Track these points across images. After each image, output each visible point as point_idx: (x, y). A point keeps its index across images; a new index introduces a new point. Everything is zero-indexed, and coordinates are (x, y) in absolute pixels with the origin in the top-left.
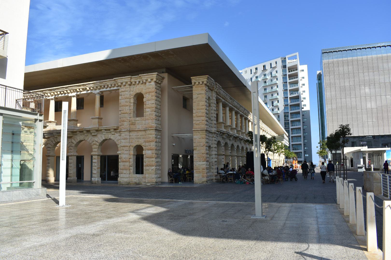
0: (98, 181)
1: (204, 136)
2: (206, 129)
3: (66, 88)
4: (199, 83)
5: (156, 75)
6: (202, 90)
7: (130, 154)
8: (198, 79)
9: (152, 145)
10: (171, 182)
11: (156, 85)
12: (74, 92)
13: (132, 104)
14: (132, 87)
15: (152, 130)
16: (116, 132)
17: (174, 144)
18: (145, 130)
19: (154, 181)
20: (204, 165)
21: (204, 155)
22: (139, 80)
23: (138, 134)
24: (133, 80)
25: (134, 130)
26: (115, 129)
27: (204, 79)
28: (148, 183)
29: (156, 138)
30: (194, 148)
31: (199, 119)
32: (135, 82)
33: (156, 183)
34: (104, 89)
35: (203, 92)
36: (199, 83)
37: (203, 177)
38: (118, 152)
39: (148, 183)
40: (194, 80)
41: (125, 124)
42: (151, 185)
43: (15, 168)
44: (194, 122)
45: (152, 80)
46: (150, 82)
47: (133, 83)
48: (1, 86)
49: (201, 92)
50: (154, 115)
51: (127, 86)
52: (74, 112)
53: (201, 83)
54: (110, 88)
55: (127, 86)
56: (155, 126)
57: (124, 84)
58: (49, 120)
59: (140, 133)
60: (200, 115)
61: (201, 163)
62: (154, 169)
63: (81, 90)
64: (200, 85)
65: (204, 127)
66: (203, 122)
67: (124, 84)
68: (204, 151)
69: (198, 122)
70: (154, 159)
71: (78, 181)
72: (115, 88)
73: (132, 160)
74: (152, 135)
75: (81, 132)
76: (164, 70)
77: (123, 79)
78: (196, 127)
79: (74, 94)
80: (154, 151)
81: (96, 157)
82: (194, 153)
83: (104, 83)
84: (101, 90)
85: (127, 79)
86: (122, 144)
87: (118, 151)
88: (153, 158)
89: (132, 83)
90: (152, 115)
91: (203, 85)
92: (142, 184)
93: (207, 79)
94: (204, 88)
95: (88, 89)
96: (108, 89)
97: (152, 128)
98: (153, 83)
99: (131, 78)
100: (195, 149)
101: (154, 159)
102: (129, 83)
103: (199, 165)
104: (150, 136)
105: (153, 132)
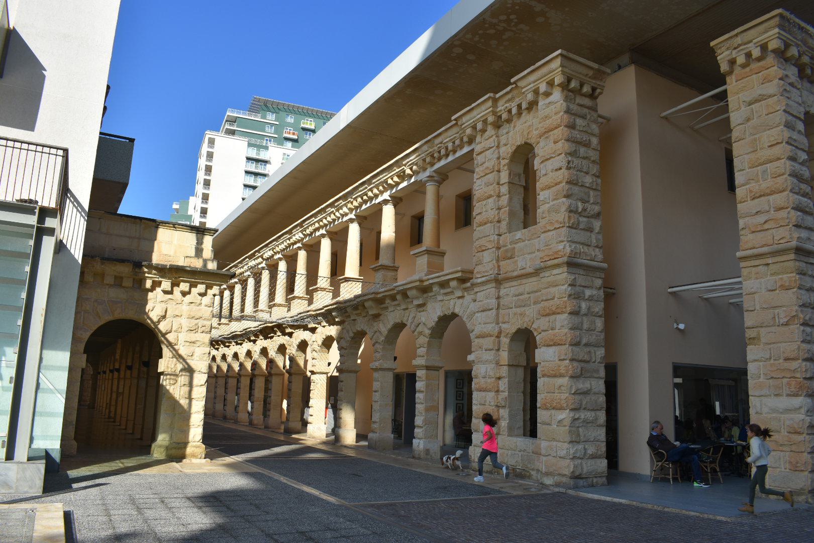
0: (427, 451)
1: (789, 277)
2: (794, 243)
3: (369, 182)
4: (749, 55)
5: (558, 62)
6: (767, 80)
7: (498, 364)
8: (739, 40)
9: (558, 325)
10: (660, 478)
11: (566, 99)
12: (385, 190)
13: (504, 189)
14: (503, 131)
15: (557, 266)
16: (466, 289)
17: (682, 326)
18: (537, 272)
19: (567, 472)
20: (797, 410)
21: (794, 365)
22: (517, 101)
23: (521, 289)
24: (501, 107)
25: (510, 275)
26: (462, 280)
27: (766, 32)
28: (547, 474)
29: (576, 296)
30: (749, 334)
31: (762, 203)
32: (510, 111)
33: (576, 477)
34: (443, 162)
35: (772, 88)
36: (749, 55)
37: (795, 469)
38: (470, 358)
39: (547, 474)
40: (727, 49)
41: (487, 256)
42: (557, 485)
43: (50, 391)
44: (741, 223)
45: (551, 84)
46: (547, 94)
47: (505, 116)
48: (3, 142)
49: (759, 92)
50: (563, 209)
51: (490, 131)
52: (388, 246)
53: (756, 53)
54: (454, 152)
55: (490, 131)
56: (568, 250)
57: (479, 126)
58: (346, 276)
59: (530, 284)
60: (765, 185)
61: (784, 402)
62: (567, 422)
63: (396, 179)
64: (754, 66)
65: (787, 236)
66: (783, 214)
67: (479, 126)
68: (794, 346)
69: (761, 219)
70: (565, 381)
71: (396, 447)
72: (466, 149)
73: (503, 385)
74: (558, 285)
75: (393, 298)
76: (626, 58)
77: (475, 113)
78: (749, 241)
79: (386, 196)
80: (565, 350)
81: (424, 372)
82: (749, 357)
83: (437, 141)
84: (436, 167)
85: (483, 107)
86: (478, 330)
87: (470, 353)
88: (562, 376)
89: (500, 117)
90: (557, 211)
91: (770, 59)
92: (530, 477)
93: (781, 27)
94: (773, 68)
95: (408, 171)
96: (451, 158)
97: (556, 261)
98: (557, 95)
99: (495, 101)
100: (755, 340)
101: (565, 381)
102: (491, 119)
103: (774, 410)
104: (553, 290)
105: (562, 275)
